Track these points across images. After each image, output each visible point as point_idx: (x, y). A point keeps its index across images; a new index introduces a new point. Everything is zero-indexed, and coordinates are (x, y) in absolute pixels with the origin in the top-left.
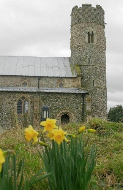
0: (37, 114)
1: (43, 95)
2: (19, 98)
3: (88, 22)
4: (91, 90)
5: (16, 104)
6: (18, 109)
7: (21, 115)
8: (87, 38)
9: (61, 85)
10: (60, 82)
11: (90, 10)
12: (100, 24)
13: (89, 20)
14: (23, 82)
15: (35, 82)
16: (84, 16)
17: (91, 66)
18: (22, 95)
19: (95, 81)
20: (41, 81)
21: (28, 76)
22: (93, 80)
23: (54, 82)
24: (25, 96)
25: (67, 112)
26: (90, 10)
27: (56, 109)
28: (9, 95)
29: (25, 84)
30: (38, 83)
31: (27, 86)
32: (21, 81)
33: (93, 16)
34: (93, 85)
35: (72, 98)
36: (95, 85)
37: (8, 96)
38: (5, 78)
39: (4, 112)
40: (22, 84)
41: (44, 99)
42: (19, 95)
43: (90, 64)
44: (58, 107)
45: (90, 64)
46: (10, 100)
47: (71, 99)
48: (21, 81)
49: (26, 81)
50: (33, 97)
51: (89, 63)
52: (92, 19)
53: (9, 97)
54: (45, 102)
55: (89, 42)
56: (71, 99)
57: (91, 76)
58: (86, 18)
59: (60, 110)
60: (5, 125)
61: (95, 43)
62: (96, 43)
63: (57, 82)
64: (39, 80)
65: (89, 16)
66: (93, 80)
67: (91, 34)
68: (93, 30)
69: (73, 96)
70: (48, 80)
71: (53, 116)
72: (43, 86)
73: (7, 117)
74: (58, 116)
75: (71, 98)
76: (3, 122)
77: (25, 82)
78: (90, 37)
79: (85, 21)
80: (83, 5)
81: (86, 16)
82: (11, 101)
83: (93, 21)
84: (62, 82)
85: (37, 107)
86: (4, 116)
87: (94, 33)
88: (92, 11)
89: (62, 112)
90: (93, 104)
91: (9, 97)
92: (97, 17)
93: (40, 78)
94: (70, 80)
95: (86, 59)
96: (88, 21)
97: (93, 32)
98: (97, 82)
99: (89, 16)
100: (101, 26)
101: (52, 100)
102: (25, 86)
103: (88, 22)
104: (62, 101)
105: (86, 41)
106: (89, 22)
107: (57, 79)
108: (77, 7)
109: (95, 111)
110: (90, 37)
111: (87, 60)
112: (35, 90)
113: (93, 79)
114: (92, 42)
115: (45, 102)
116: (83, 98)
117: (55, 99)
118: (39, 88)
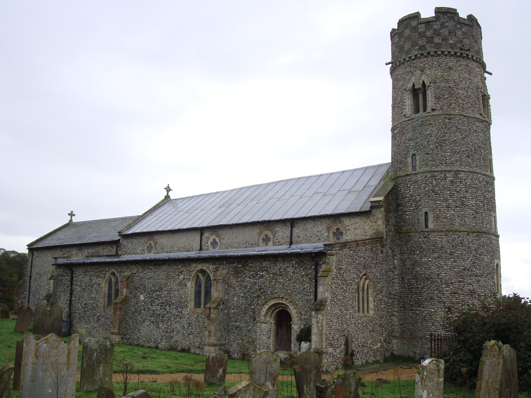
0: (210, 309)
1: (236, 264)
2: (194, 273)
3: (436, 60)
4: (420, 240)
5: (190, 286)
7: (198, 309)
10: (335, 227)
11: (415, 29)
12: (446, 55)
14: (263, 236)
17: (419, 176)
18: (200, 267)
20: (296, 231)
21: (269, 222)
22: (426, 213)
25: (280, 303)
26: (415, 29)
27: (259, 297)
28: (180, 267)
29: (266, 240)
30: (289, 235)
31: (271, 243)
32: (260, 234)
34: (426, 226)
35: (293, 267)
36: (431, 225)
37: (179, 269)
38: (176, 235)
39: (173, 304)
40: (261, 241)
42: (194, 265)
43: (418, 170)
44: (264, 291)
45: (418, 170)
46: (182, 277)
47: (290, 270)
48: (260, 234)
49: (270, 235)
51: (414, 168)
52: (422, 48)
53: (181, 272)
54: (239, 280)
55: (417, 111)
57: (420, 201)
60: (173, 331)
61: (429, 109)
62: (433, 110)
63: (329, 229)
64: (292, 227)
66: (426, 213)
67: (419, 89)
68: (423, 78)
69: (294, 262)
70: (309, 225)
71: (254, 313)
72: (301, 241)
73: (177, 315)
74: (263, 313)
75: (290, 268)
76: (171, 324)
77: (266, 235)
79: (405, 59)
80: (401, 22)
82: (183, 279)
83: (422, 54)
84: (339, 226)
85: (217, 293)
86: (173, 313)
87: (427, 84)
89: (272, 302)
90: (427, 278)
91: (181, 272)
92: (437, 40)
93: (292, 222)
94: (357, 220)
95: (406, 158)
96: (410, 58)
97: (424, 84)
98: (437, 218)
100: (473, 65)
101: (252, 275)
102: (266, 244)
104: (271, 275)
106: (414, 59)
107: (328, 222)
109: (431, 298)
111: (409, 159)
112: (283, 249)
113: (425, 210)
115: (239, 280)
117: (258, 271)
118: (292, 246)
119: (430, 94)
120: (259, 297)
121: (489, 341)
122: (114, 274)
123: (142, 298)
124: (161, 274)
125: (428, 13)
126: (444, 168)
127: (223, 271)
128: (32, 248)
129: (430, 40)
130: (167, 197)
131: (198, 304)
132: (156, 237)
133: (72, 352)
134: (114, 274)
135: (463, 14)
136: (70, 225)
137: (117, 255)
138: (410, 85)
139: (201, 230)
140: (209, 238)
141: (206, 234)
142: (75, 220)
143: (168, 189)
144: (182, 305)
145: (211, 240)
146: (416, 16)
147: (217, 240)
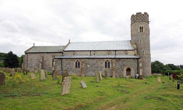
3: (140, 21)
5: (104, 63)
6: (105, 66)
8: (139, 30)
9: (126, 54)
11: (141, 15)
13: (140, 21)
14: (108, 53)
15: (113, 53)
16: (137, 19)
18: (107, 60)
19: (144, 51)
20: (116, 52)
23: (123, 52)
24: (108, 60)
33: (142, 18)
36: (144, 53)
41: (117, 61)
46: (101, 62)
47: (131, 61)
49: (110, 53)
50: (112, 60)
52: (142, 20)
56: (131, 61)
58: (139, 20)
59: (126, 66)
65: (140, 19)
70: (120, 51)
75: (131, 60)
78: (141, 29)
81: (139, 19)
87: (143, 27)
88: (142, 16)
93: (116, 51)
98: (145, 52)
99: (140, 19)
100: (147, 23)
103: (140, 21)
105: (139, 31)
107: (125, 51)
108: (133, 15)
110: (141, 29)
114: (142, 32)
116: (138, 60)
119: (144, 29)
120: (123, 66)
121: (12, 68)
122: (78, 61)
123: (89, 66)
124: (95, 61)
125: (135, 14)
126: (146, 43)
127: (114, 61)
128: (26, 53)
129: (144, 18)
130: (69, 42)
131: (106, 67)
132: (76, 52)
133: (132, 82)
134: (78, 61)
135: (143, 13)
136: (33, 47)
137: (62, 55)
138: (140, 27)
139: (91, 51)
140: (93, 53)
141: (92, 52)
142: (35, 45)
143: (69, 40)
144: (101, 67)
145: (93, 53)
146: (141, 13)
147: (95, 53)
